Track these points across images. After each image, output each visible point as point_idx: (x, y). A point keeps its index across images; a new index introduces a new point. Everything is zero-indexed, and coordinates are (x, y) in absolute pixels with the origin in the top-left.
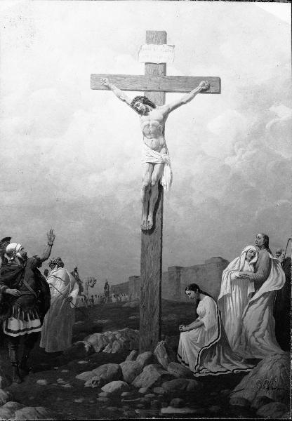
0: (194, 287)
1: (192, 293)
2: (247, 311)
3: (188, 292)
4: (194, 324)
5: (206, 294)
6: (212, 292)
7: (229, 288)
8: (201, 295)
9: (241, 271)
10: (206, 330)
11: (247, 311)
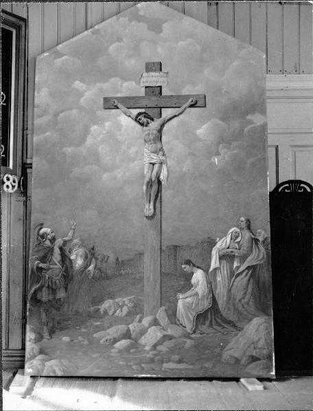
0: (188, 262)
1: (187, 267)
2: (234, 281)
3: (183, 266)
4: (189, 293)
5: (198, 268)
6: (203, 266)
7: (218, 262)
8: (195, 268)
9: (228, 248)
10: (200, 297)
11: (234, 281)
